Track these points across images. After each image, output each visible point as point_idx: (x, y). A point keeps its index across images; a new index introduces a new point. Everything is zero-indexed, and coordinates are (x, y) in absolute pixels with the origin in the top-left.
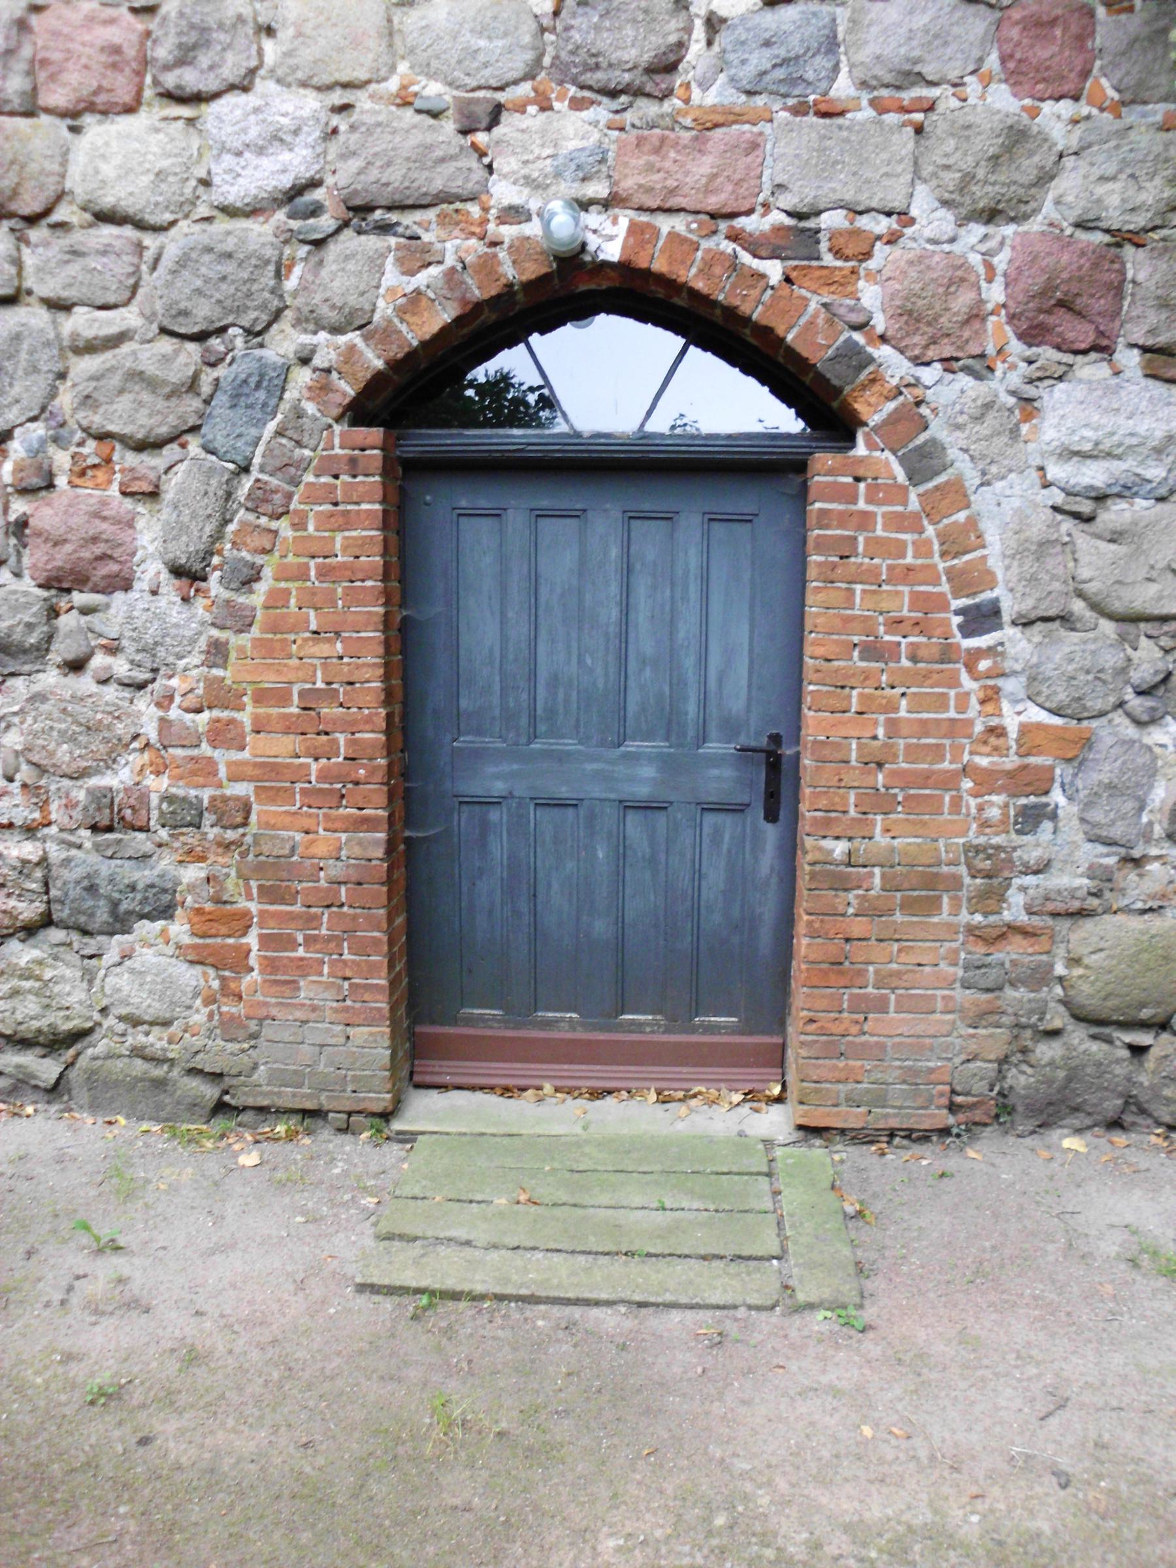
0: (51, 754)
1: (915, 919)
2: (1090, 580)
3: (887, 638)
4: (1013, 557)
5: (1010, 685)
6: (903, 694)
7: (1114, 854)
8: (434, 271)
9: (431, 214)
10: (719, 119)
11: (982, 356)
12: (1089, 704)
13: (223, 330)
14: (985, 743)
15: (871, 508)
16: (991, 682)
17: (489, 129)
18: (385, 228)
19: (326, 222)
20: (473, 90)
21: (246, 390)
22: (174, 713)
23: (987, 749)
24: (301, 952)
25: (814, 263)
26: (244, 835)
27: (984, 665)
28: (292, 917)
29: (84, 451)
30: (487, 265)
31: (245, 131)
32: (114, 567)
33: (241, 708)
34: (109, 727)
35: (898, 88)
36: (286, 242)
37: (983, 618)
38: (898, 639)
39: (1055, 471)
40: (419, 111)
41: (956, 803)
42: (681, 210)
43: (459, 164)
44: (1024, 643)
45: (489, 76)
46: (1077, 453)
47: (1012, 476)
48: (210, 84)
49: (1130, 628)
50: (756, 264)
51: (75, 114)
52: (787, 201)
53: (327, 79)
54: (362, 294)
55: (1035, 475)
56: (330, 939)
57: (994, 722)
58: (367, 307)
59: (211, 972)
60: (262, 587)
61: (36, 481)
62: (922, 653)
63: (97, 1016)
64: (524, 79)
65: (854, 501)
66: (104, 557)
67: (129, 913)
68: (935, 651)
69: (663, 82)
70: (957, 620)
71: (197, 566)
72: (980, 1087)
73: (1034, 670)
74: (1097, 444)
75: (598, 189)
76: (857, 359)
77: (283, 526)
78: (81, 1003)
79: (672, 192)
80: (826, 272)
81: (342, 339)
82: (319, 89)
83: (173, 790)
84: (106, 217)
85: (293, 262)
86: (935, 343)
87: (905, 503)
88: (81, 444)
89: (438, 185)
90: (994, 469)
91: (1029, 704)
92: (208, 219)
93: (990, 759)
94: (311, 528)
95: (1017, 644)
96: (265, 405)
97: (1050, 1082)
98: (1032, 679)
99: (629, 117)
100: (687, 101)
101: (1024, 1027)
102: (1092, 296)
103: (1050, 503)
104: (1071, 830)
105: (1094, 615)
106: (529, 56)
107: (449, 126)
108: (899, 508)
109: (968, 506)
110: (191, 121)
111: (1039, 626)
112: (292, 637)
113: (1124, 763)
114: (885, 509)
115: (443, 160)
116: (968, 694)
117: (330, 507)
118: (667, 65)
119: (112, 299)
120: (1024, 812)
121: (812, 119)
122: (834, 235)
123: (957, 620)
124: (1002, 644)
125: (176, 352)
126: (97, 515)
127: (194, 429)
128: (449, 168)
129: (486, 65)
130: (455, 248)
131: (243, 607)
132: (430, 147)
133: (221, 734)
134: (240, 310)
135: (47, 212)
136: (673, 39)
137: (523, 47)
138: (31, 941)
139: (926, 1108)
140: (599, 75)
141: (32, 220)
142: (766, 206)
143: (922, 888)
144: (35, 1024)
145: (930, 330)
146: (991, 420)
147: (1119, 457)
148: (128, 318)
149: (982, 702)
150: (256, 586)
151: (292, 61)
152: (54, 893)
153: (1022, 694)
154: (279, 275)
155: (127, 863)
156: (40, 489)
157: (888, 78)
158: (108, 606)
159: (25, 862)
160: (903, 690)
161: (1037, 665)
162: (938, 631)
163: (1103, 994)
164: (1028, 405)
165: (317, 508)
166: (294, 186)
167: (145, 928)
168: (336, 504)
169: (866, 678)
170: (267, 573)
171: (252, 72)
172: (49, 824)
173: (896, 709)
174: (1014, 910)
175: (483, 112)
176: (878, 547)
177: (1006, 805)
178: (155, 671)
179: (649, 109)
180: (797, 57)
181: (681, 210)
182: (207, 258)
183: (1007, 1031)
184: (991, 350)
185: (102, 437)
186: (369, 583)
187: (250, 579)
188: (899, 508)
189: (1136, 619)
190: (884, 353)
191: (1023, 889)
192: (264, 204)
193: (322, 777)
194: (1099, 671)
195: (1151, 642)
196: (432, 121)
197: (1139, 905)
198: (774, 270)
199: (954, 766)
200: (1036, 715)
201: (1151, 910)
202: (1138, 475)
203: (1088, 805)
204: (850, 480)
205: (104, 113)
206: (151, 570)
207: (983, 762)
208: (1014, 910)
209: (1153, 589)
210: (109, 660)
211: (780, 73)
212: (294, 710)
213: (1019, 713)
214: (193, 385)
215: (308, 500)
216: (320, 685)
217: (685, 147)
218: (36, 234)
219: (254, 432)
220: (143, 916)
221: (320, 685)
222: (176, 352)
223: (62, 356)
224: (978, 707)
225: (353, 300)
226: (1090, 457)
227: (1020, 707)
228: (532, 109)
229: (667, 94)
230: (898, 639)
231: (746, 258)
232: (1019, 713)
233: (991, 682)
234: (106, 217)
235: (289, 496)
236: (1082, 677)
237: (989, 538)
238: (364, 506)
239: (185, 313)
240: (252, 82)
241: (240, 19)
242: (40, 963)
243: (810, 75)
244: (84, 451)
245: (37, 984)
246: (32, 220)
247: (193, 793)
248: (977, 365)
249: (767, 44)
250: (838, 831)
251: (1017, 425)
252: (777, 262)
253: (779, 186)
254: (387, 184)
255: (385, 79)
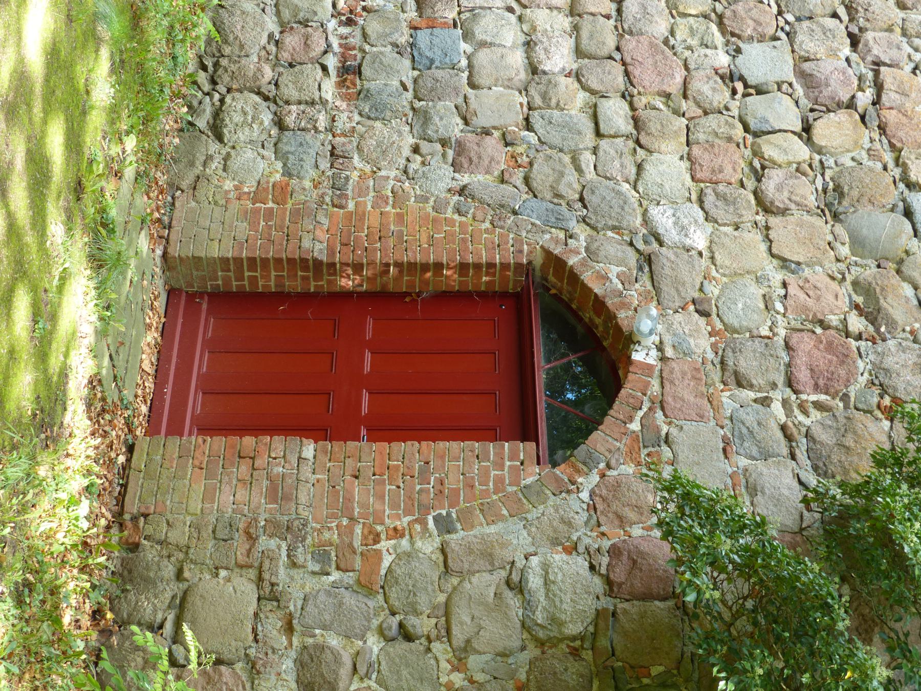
0: (371, 138)
1: (264, 490)
2: (470, 583)
3: (432, 478)
4: (483, 539)
5: (405, 543)
6: (399, 487)
7: (296, 610)
8: (620, 286)
9: (649, 287)
10: (715, 403)
11: (599, 525)
12: (394, 589)
13: (585, 207)
14: (370, 532)
15: (506, 469)
16: (407, 532)
17: (697, 311)
18: (640, 269)
19: (641, 246)
20: (716, 306)
21: (555, 214)
22: (392, 182)
23: (366, 532)
24: (262, 223)
25: (641, 445)
26: (327, 205)
27: (418, 527)
28: (283, 220)
29: (524, 157)
30: (624, 305)
31: (686, 217)
32: (466, 166)
33: (394, 207)
34: (384, 159)
35: (747, 487)
36: (631, 231)
37: (445, 525)
38: (432, 483)
39: (534, 561)
40: (702, 283)
41: (334, 516)
42: (663, 388)
43: (676, 297)
44: (431, 549)
45: (723, 309)
46: (547, 573)
47: (530, 539)
48: (707, 206)
49: (441, 612)
50: (638, 418)
51: (689, 159)
52: (674, 431)
53: (715, 248)
54: (606, 257)
55: (532, 550)
56: (270, 235)
57: (383, 536)
58: (599, 259)
59: (253, 189)
60: (456, 217)
61: (509, 138)
62: (424, 495)
63: (231, 144)
64: (724, 324)
65: (511, 460)
66: (471, 160)
67: (288, 159)
68: (425, 502)
69: (731, 380)
70: (444, 512)
71: (466, 192)
72: (149, 530)
73: (414, 555)
74: (553, 582)
75: (669, 352)
76: (589, 463)
77: (487, 225)
78: (238, 138)
79: (672, 382)
80: (637, 450)
81: (583, 250)
82: (710, 247)
83: (351, 181)
84: (640, 167)
85: (622, 235)
86: (603, 500)
87: (510, 485)
88: (527, 156)
89: (665, 288)
90: (534, 529)
91: (394, 556)
92: (641, 205)
93: (360, 534)
94: (485, 236)
95: (428, 547)
96: (548, 221)
97: (148, 568)
98: (409, 555)
99: (709, 366)
100: (722, 391)
101: (187, 553)
102: (642, 579)
103: (516, 559)
104: (311, 584)
105: (450, 590)
106: (736, 325)
107: (696, 295)
108: (507, 482)
109: (510, 516)
110: (689, 200)
111: (441, 558)
112: (430, 227)
113: (355, 612)
114: (507, 475)
115: (677, 290)
116: (400, 519)
117: (497, 242)
118: (741, 382)
119: (599, 168)
120: (327, 554)
121: (721, 445)
122: (659, 454)
123: (444, 512)
124: (430, 536)
125: (574, 190)
126: (492, 159)
127: (535, 196)
128: (673, 292)
129: (729, 308)
130: (633, 295)
131: (446, 208)
132: (684, 284)
133: (380, 199)
134: (595, 213)
135: (641, 146)
136: (754, 382)
137: (740, 322)
138: (272, 123)
139: (139, 500)
140: (730, 354)
141: (637, 142)
142: (670, 423)
143: (279, 492)
144: (227, 120)
145: (611, 497)
146: (562, 527)
147: (547, 595)
148: (590, 174)
149: (395, 529)
150: (457, 215)
151: (722, 236)
152: (299, 132)
153: (399, 551)
154: (614, 228)
155: (314, 160)
156: (505, 140)
157: (751, 480)
158: (446, 163)
159: (316, 121)
160: (402, 485)
161: (418, 557)
162: (436, 503)
163: (205, 594)
164: (572, 549)
165: (496, 238)
166: (659, 234)
167: (279, 165)
168: (499, 246)
169: (408, 468)
170: (464, 219)
171: (716, 222)
172: (334, 136)
173: (390, 484)
174: (266, 543)
175: (705, 307)
176: (485, 473)
177: (331, 545)
178: (413, 179)
179: (716, 376)
180: (754, 437)
181: (663, 388)
182: (621, 202)
183: (185, 543)
184: (603, 529)
185: (531, 164)
186: (458, 258)
187: (458, 211)
188: (507, 482)
189: (447, 614)
190: (595, 478)
191: (279, 547)
192: (650, 225)
193: (356, 238)
194: (414, 593)
195: (433, 625)
196: (697, 287)
197: (260, 628)
198: (635, 426)
199: (356, 513)
200: (387, 561)
201: (256, 635)
202: (537, 607)
203: (328, 594)
204: (522, 458)
205: (691, 169)
206: (465, 179)
207: (358, 530)
208: (266, 543)
209: (468, 620)
210: (419, 162)
211: (744, 431)
212: (392, 227)
213: (388, 550)
214: (558, 196)
215: (501, 236)
216: (405, 238)
217: (697, 389)
218: (631, 144)
219: (535, 216)
220: (285, 165)
221: (405, 238)
222: (574, 190)
223: (571, 151)
224: (392, 526)
225: (602, 253)
226: (545, 580)
227: (391, 551)
228: (709, 328)
229: (724, 383)
230: (432, 483)
231: (640, 413)
232: (388, 550)
233: (407, 532)
234: (640, 167)
235: (502, 228)
236: (410, 582)
237: (492, 527)
238: (498, 256)
239: (593, 192)
240: (711, 221)
241: (741, 216)
242: (262, 123)
243: (746, 444)
244: (524, 157)
245: (250, 122)
246: (637, 142)
247: (350, 188)
248: (593, 521)
249: (759, 424)
250: (319, 456)
251: (562, 544)
252: (640, 428)
253: (682, 428)
254: (663, 269)
255: (717, 271)
